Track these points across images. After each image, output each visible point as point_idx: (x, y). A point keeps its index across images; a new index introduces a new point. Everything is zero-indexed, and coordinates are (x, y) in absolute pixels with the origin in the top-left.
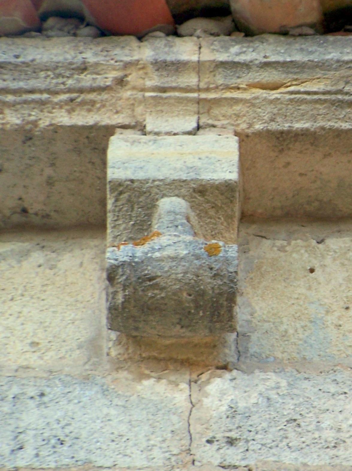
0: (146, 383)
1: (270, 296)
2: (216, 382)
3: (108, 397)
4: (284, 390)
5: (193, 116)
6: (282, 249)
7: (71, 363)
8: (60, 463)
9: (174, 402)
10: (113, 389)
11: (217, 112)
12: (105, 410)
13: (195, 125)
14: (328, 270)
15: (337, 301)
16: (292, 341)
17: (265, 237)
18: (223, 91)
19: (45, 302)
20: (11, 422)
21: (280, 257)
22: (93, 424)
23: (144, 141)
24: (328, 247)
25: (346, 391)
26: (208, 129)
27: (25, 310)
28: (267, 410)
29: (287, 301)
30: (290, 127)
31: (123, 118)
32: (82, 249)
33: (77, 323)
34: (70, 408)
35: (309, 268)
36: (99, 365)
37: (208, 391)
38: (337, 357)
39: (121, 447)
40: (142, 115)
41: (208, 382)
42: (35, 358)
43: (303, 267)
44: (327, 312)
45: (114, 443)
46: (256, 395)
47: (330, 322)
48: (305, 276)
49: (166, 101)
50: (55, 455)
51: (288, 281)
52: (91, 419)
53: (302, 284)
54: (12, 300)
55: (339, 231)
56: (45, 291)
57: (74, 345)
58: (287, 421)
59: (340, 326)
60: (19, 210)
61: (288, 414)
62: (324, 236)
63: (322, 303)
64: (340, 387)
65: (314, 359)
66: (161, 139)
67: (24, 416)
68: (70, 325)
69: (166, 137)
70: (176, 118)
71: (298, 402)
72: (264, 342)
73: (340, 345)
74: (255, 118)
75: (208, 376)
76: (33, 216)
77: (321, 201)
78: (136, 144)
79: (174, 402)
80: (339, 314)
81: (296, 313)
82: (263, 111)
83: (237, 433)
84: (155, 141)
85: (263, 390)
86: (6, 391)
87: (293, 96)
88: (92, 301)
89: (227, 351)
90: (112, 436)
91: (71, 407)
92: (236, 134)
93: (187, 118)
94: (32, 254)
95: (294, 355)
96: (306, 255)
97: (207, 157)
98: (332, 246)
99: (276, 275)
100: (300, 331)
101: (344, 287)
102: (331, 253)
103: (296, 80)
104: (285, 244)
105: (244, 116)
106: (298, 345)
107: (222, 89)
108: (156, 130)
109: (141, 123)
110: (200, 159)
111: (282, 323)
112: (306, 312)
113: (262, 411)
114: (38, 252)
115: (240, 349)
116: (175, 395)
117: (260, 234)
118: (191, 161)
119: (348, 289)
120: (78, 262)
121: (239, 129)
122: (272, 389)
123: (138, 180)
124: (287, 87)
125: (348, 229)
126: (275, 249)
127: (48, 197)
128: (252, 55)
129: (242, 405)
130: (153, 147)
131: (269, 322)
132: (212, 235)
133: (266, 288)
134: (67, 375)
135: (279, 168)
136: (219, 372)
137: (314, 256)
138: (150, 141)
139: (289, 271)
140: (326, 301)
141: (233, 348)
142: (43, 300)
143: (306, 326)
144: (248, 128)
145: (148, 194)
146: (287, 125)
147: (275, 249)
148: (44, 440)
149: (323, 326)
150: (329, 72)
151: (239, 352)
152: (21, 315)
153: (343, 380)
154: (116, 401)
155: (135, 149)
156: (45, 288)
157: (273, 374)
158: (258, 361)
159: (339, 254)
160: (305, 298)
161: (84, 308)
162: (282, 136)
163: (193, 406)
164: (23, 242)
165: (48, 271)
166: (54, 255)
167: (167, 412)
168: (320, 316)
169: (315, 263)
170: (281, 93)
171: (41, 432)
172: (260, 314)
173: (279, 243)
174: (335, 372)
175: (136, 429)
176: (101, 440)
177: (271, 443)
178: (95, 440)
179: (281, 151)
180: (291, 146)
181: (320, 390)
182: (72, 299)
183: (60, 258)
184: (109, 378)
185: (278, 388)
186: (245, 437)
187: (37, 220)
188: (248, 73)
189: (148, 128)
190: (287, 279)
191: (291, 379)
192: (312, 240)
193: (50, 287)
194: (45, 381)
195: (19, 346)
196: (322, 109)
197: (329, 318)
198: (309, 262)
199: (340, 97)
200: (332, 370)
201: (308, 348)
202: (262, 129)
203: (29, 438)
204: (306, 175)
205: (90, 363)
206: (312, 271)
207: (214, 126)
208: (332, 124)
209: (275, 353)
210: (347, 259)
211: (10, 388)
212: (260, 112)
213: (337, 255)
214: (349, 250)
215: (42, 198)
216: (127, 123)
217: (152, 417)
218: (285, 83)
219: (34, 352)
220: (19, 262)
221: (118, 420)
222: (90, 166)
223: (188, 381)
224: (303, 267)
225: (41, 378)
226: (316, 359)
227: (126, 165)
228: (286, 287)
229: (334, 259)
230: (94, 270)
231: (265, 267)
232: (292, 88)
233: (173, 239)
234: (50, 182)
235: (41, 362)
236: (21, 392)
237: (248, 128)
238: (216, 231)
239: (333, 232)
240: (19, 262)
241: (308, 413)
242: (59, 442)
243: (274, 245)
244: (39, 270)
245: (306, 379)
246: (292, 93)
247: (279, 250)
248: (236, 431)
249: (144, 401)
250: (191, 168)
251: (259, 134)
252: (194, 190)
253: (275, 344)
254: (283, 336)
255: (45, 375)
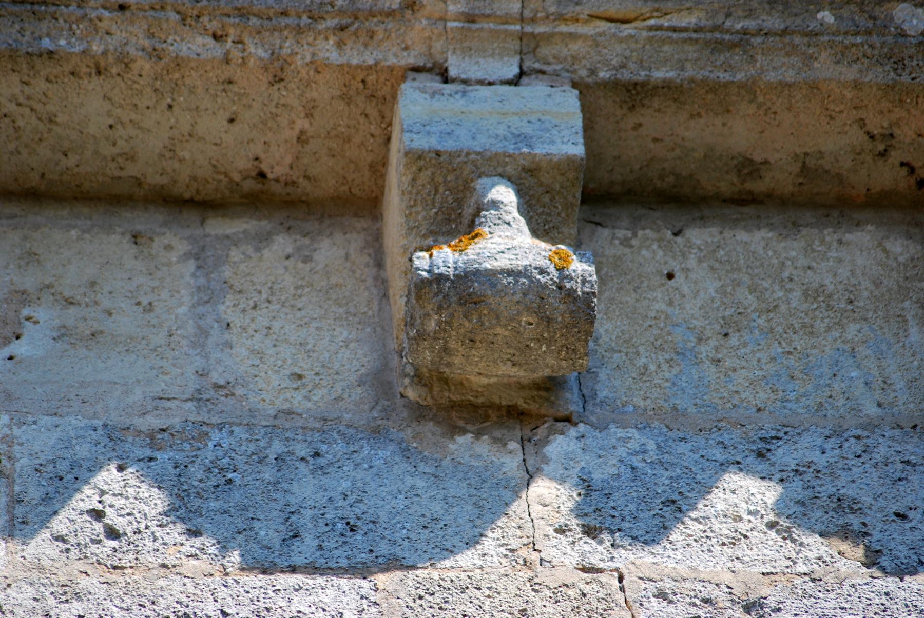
0: (460, 440)
1: (617, 313)
2: (558, 441)
3: (411, 460)
4: (652, 456)
5: (513, 57)
6: (626, 242)
7: (352, 407)
8: (354, 560)
9: (504, 470)
10: (416, 448)
11: (547, 52)
12: (409, 481)
13: (516, 70)
14: (693, 276)
15: (710, 324)
18: (556, 23)
19: (303, 312)
20: (278, 496)
21: (624, 255)
22: (394, 501)
23: (448, 92)
24: (688, 241)
25: (738, 459)
26: (533, 76)
27: (276, 325)
28: (632, 484)
29: (641, 322)
31: (415, 57)
32: (345, 233)
33: (352, 345)
34: (359, 477)
35: (666, 272)
36: (394, 410)
37: (548, 454)
38: (720, 408)
39: (437, 536)
40: (443, 53)
41: (546, 441)
42: (300, 398)
43: (658, 271)
44: (700, 340)
45: (427, 531)
46: (614, 462)
47: (705, 355)
48: (663, 285)
49: (476, 34)
50: (346, 548)
51: (639, 291)
52: (390, 493)
53: (660, 296)
54: (255, 307)
55: (702, 218)
56: (300, 297)
57: (353, 378)
60: (254, 174)
61: (664, 492)
62: (682, 223)
63: (691, 326)
65: (689, 410)
66: (472, 91)
67: (295, 487)
68: (343, 350)
69: (478, 87)
70: (490, 60)
71: (673, 474)
72: (617, 383)
73: (722, 390)
74: (599, 62)
75: (546, 433)
76: (273, 182)
77: (677, 176)
78: (437, 96)
79: (504, 470)
80: (716, 343)
84: (464, 93)
85: (625, 455)
86: (265, 448)
87: (652, 34)
88: (370, 313)
89: (568, 395)
90: (422, 519)
91: (360, 475)
92: (575, 85)
93: (506, 59)
94: (274, 237)
95: (662, 403)
96: (660, 253)
97: (539, 120)
98: (694, 240)
100: (665, 367)
102: (694, 251)
103: (657, 10)
105: (584, 58)
106: (665, 388)
107: (554, 20)
108: (463, 76)
109: (441, 65)
110: (529, 122)
111: (638, 354)
112: (670, 338)
114: (282, 235)
115: (585, 391)
116: (502, 460)
117: (593, 219)
118: (520, 125)
119: (724, 306)
120: (342, 253)
121: (576, 78)
123: (446, 152)
124: (645, 20)
126: (617, 242)
127: (297, 158)
129: (597, 476)
130: (462, 102)
131: (620, 352)
132: (545, 230)
133: (611, 300)
134: (348, 426)
136: (560, 425)
138: (456, 93)
140: (694, 321)
141: (576, 390)
142: (299, 309)
143: (672, 360)
145: (458, 172)
146: (643, 73)
147: (617, 242)
148: (327, 525)
151: (583, 396)
152: (271, 332)
154: (422, 467)
155: (438, 104)
156: (299, 291)
157: (634, 431)
159: (705, 252)
160: (666, 318)
161: (360, 323)
162: (635, 88)
163: (531, 477)
164: (259, 219)
165: (300, 265)
166: (307, 241)
167: (495, 485)
169: (674, 265)
170: (636, 28)
171: (322, 512)
172: (607, 340)
173: (621, 233)
175: (455, 509)
176: (408, 525)
178: (399, 525)
179: (632, 108)
180: (646, 102)
181: (702, 456)
182: (341, 310)
183: (316, 245)
184: (409, 431)
185: (645, 452)
186: (607, 525)
187: (277, 188)
189: (453, 73)
190: (638, 288)
192: (665, 230)
193: (307, 290)
194: (318, 434)
195: (275, 381)
199: (718, 35)
200: (716, 426)
201: (679, 393)
202: (610, 78)
203: (305, 519)
204: (662, 140)
205: (379, 408)
206: (670, 276)
207: (543, 72)
208: (707, 74)
210: (717, 260)
211: (270, 444)
212: (606, 54)
214: (718, 247)
215: (288, 160)
216: (422, 64)
217: (475, 492)
219: (297, 389)
220: (258, 250)
221: (428, 495)
222: (362, 120)
223: (519, 439)
224: (658, 271)
225: (312, 430)
226: (692, 410)
227: (428, 128)
228: (637, 300)
229: (700, 261)
230: (367, 265)
231: (605, 269)
232: (652, 22)
233: (506, 244)
234: (302, 139)
235: (309, 405)
236: (286, 450)
237: (588, 77)
238: (551, 225)
239: (693, 219)
240: (258, 250)
241: (689, 491)
242: (348, 528)
243: (614, 237)
244: (287, 263)
245: (681, 440)
246: (651, 28)
247: (621, 244)
248: (594, 516)
249: (460, 468)
250: (519, 136)
252: (524, 169)
253: (633, 387)
254: (643, 374)
255: (317, 425)
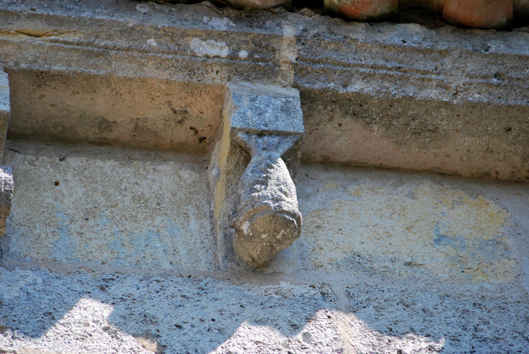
6: (32, 163)
14: (70, 184)
16: (44, 244)
17: (17, 151)
24: (68, 164)
30: (48, 68)
48: (52, 188)
51: (38, 191)
53: (50, 195)
55: (77, 152)
58: (44, 314)
59: (82, 234)
61: (45, 307)
62: (65, 154)
64: (85, 287)
65: (63, 261)
71: (51, 298)
72: (22, 244)
73: (83, 251)
77: (64, 127)
81: (46, 220)
82: (28, 53)
83: (4, 322)
85: (23, 285)
87: (52, 44)
96: (52, 170)
99: (28, 185)
100: (50, 236)
101: (84, 201)
102: (71, 170)
104: (34, 159)
106: (49, 248)
113: (23, 304)
117: (13, 149)
122: (30, 285)
125: (84, 150)
126: (26, 162)
128: (21, 6)
131: (25, 226)
133: (21, 196)
135: (35, 99)
137: (58, 171)
139: (39, 182)
143: (55, 232)
144: (14, 66)
149: (68, 233)
150: (83, 28)
153: (87, 280)
157: (30, 271)
158: (17, 259)
160: (53, 208)
162: (41, 75)
168: (66, 224)
169: (59, 177)
170: (43, 40)
173: (29, 157)
174: (80, 273)
177: (32, 332)
179: (39, 86)
180: (47, 83)
181: (69, 288)
188: (18, 21)
191: (45, 277)
196: (75, 56)
197: (73, 226)
198: (55, 176)
201: (58, 251)
206: (57, 184)
209: (32, 254)
213: (76, 172)
218: (47, 33)
226: (65, 261)
229: (74, 176)
237: (14, 66)
241: (60, 308)
245: (57, 278)
246: (52, 41)
251: (24, 71)
